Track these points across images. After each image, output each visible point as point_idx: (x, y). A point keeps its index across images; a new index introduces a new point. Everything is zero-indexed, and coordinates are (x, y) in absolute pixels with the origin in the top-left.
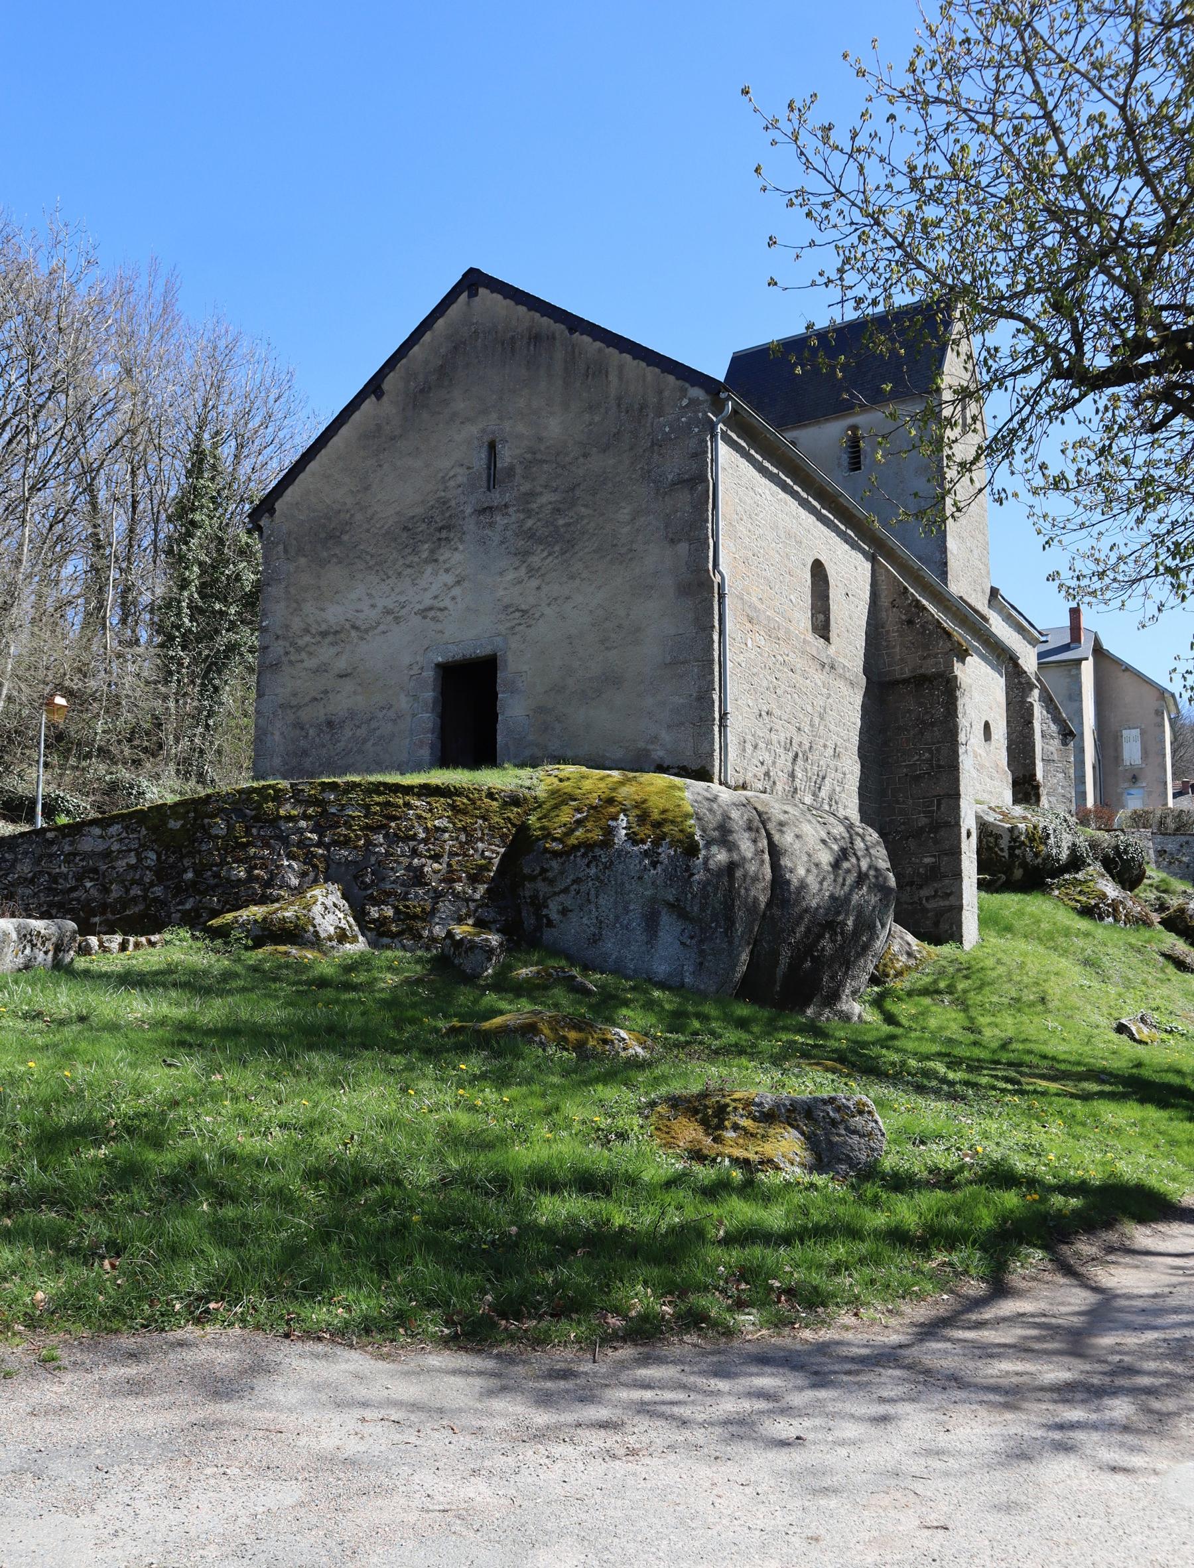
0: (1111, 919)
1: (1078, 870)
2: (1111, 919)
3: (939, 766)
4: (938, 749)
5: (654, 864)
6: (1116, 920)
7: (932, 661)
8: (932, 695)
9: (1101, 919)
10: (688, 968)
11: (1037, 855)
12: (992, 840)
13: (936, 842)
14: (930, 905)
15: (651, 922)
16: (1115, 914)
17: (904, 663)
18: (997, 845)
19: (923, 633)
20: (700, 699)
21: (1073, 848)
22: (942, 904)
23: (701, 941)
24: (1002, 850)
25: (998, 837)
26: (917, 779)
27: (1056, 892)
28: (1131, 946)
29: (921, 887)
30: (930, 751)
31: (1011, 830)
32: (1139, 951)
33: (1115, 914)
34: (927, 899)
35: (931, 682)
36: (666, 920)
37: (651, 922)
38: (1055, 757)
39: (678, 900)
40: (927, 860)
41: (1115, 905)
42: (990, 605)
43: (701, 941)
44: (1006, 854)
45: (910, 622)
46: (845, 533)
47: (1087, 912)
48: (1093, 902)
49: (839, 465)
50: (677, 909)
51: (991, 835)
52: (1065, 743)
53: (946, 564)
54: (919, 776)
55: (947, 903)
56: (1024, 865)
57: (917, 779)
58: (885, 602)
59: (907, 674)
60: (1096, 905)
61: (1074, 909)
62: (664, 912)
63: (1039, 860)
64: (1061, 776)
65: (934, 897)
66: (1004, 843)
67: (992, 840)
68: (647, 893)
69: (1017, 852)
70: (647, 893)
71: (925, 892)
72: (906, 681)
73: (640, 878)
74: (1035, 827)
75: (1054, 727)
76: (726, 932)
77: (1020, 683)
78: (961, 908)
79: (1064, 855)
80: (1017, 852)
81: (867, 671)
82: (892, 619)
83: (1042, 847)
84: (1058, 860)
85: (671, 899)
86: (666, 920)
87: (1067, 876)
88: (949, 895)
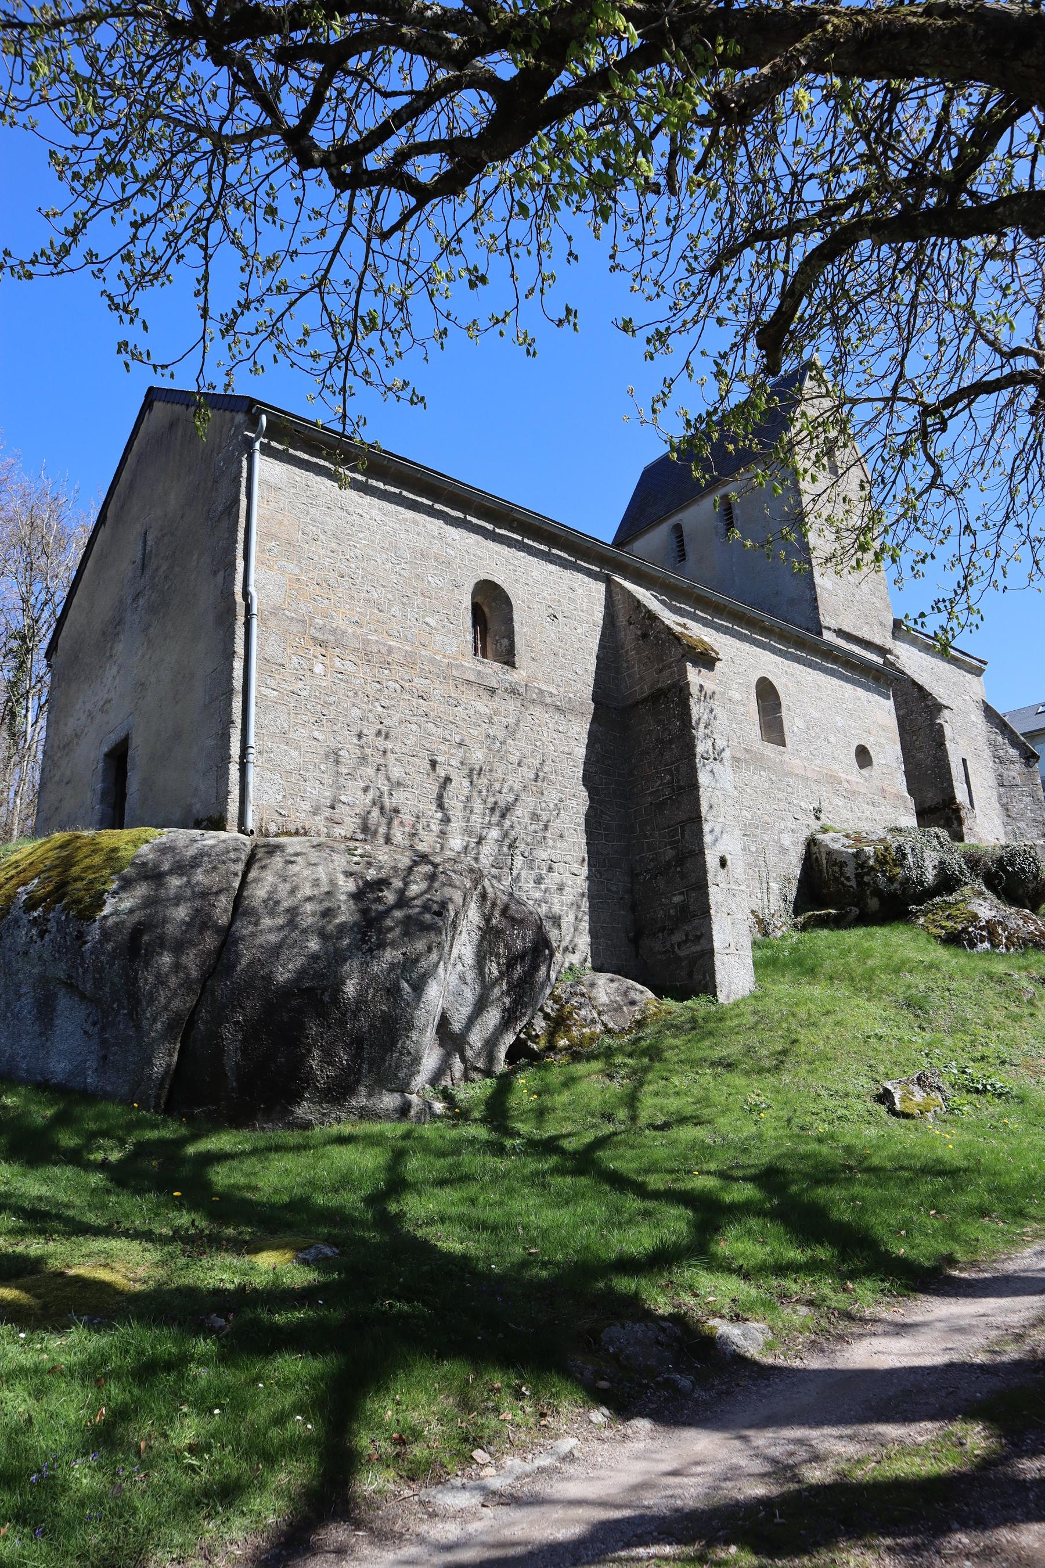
0: (986, 945)
1: (951, 891)
2: (986, 945)
3: (680, 788)
4: (677, 769)
5: (42, 935)
6: (994, 946)
7: (666, 673)
8: (668, 709)
9: (972, 946)
10: (92, 1064)
11: (891, 880)
12: (836, 869)
13: (683, 876)
14: (682, 953)
15: (45, 1009)
16: (992, 937)
17: (641, 680)
18: (842, 874)
19: (657, 644)
20: (223, 734)
21: (942, 867)
22: (694, 949)
23: (103, 1029)
24: (848, 879)
25: (843, 865)
26: (660, 806)
27: (922, 920)
28: (990, 976)
29: (672, 932)
30: (670, 772)
31: (857, 855)
32: (1000, 981)
33: (992, 937)
34: (679, 945)
35: (666, 695)
36: (64, 1002)
37: (45, 1009)
38: (1019, 781)
39: (70, 977)
40: (677, 899)
41: (990, 928)
42: (894, 636)
43: (103, 1029)
44: (853, 883)
45: (645, 636)
46: (549, 554)
47: (953, 940)
48: (960, 927)
49: (717, 534)
50: (71, 986)
51: (835, 864)
52: (1028, 765)
53: (816, 599)
54: (663, 803)
55: (698, 948)
56: (877, 892)
57: (660, 806)
58: (622, 621)
59: (647, 692)
60: (965, 930)
61: (936, 937)
62: (61, 994)
63: (896, 885)
64: (1028, 799)
65: (685, 942)
66: (850, 871)
67: (836, 869)
68: (35, 971)
69: (866, 879)
70: (35, 971)
71: (677, 937)
72: (645, 700)
73: (26, 953)
74: (886, 849)
75: (1013, 752)
76: (130, 1014)
77: (927, 706)
78: (711, 952)
79: (930, 876)
80: (866, 879)
81: (597, 698)
82: (628, 636)
83: (898, 870)
84: (921, 883)
85: (62, 976)
86: (64, 1002)
87: (937, 899)
88: (698, 938)
